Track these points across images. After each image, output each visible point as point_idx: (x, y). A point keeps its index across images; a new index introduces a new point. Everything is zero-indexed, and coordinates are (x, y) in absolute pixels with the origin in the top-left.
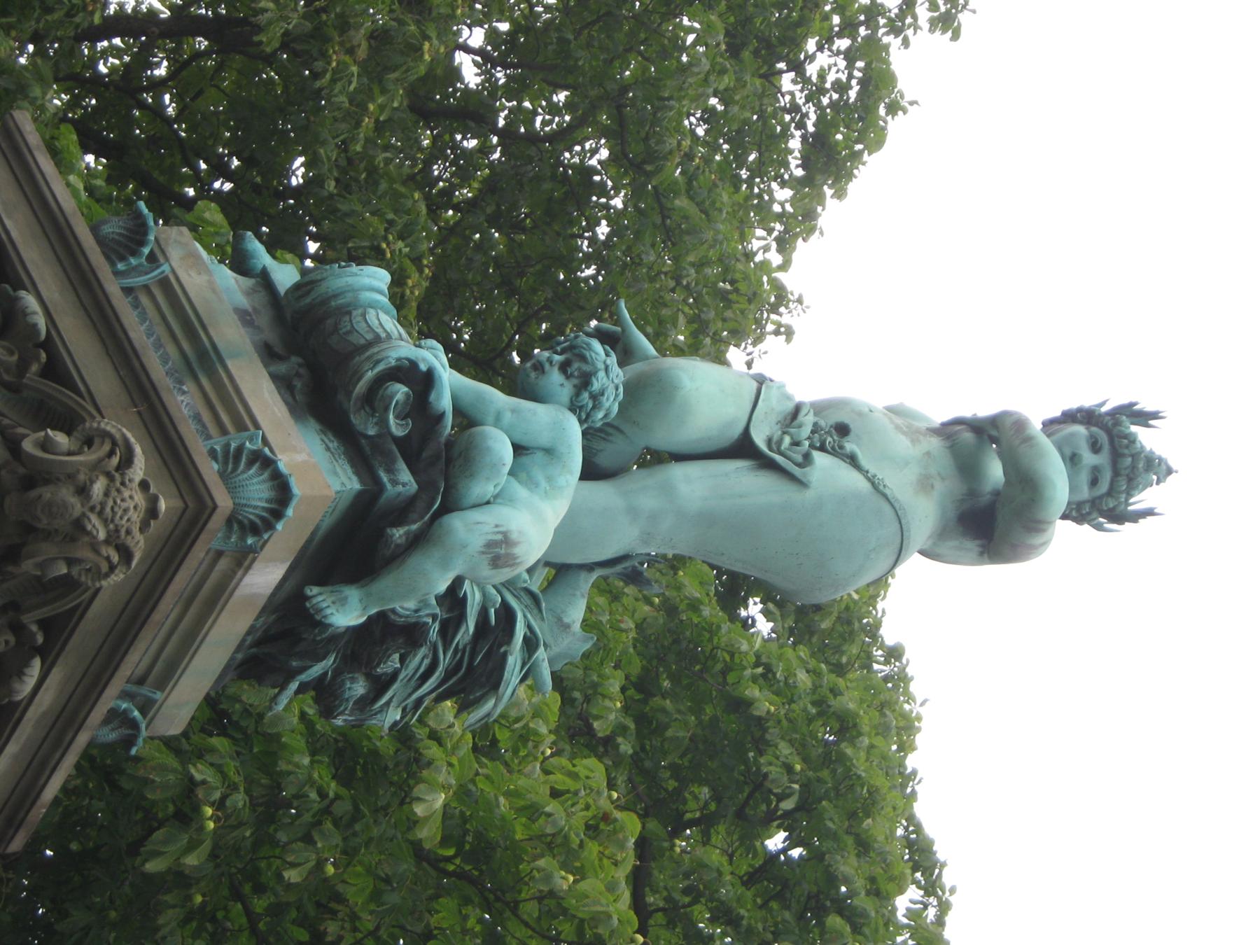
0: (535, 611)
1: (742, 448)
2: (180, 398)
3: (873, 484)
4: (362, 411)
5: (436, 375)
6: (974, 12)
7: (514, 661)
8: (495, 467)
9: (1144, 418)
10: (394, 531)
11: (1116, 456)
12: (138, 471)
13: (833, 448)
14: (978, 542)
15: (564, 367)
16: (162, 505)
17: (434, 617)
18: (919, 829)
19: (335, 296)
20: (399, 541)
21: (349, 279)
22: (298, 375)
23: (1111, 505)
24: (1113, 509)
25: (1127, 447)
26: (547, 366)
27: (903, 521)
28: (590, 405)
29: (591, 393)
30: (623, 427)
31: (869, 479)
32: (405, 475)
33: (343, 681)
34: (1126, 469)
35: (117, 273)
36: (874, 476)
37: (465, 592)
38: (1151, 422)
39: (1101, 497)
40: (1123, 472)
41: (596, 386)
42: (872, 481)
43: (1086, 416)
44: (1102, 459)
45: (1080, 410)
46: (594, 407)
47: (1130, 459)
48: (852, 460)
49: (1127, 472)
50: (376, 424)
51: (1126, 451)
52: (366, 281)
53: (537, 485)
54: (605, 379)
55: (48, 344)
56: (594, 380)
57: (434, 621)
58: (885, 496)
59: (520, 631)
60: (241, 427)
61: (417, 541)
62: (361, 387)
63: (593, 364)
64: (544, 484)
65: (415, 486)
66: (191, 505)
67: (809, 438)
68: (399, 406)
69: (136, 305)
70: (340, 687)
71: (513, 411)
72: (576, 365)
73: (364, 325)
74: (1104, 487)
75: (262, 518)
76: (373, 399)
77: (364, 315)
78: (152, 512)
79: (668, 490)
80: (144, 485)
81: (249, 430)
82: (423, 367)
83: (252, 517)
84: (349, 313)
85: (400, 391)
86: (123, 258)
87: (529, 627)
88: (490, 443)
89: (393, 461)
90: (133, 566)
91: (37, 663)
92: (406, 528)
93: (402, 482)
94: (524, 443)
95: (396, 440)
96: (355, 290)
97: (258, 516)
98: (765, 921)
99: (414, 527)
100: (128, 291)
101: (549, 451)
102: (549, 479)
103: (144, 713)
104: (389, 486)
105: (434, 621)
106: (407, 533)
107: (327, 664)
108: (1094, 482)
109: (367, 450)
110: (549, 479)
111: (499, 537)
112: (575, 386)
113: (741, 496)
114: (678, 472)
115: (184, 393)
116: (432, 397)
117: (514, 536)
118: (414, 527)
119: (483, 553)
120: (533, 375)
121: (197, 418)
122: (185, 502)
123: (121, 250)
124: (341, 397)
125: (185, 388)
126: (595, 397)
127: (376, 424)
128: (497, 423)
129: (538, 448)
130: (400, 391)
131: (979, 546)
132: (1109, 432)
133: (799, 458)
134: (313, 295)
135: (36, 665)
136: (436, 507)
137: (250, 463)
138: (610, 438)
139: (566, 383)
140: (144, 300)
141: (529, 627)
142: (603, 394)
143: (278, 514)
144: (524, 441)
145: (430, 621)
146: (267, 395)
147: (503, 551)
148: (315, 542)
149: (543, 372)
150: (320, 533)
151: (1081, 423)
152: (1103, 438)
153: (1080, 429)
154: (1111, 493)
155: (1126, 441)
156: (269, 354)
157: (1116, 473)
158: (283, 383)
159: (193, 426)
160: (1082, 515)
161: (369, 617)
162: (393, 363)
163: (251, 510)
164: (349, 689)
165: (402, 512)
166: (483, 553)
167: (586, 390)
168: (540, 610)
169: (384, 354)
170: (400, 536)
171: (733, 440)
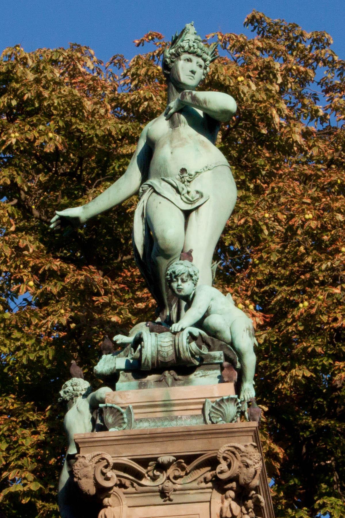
1: (187, 214)
11: (194, 53)
12: (242, 448)
15: (183, 281)
55: (178, 457)
80: (246, 446)
137: (220, 406)
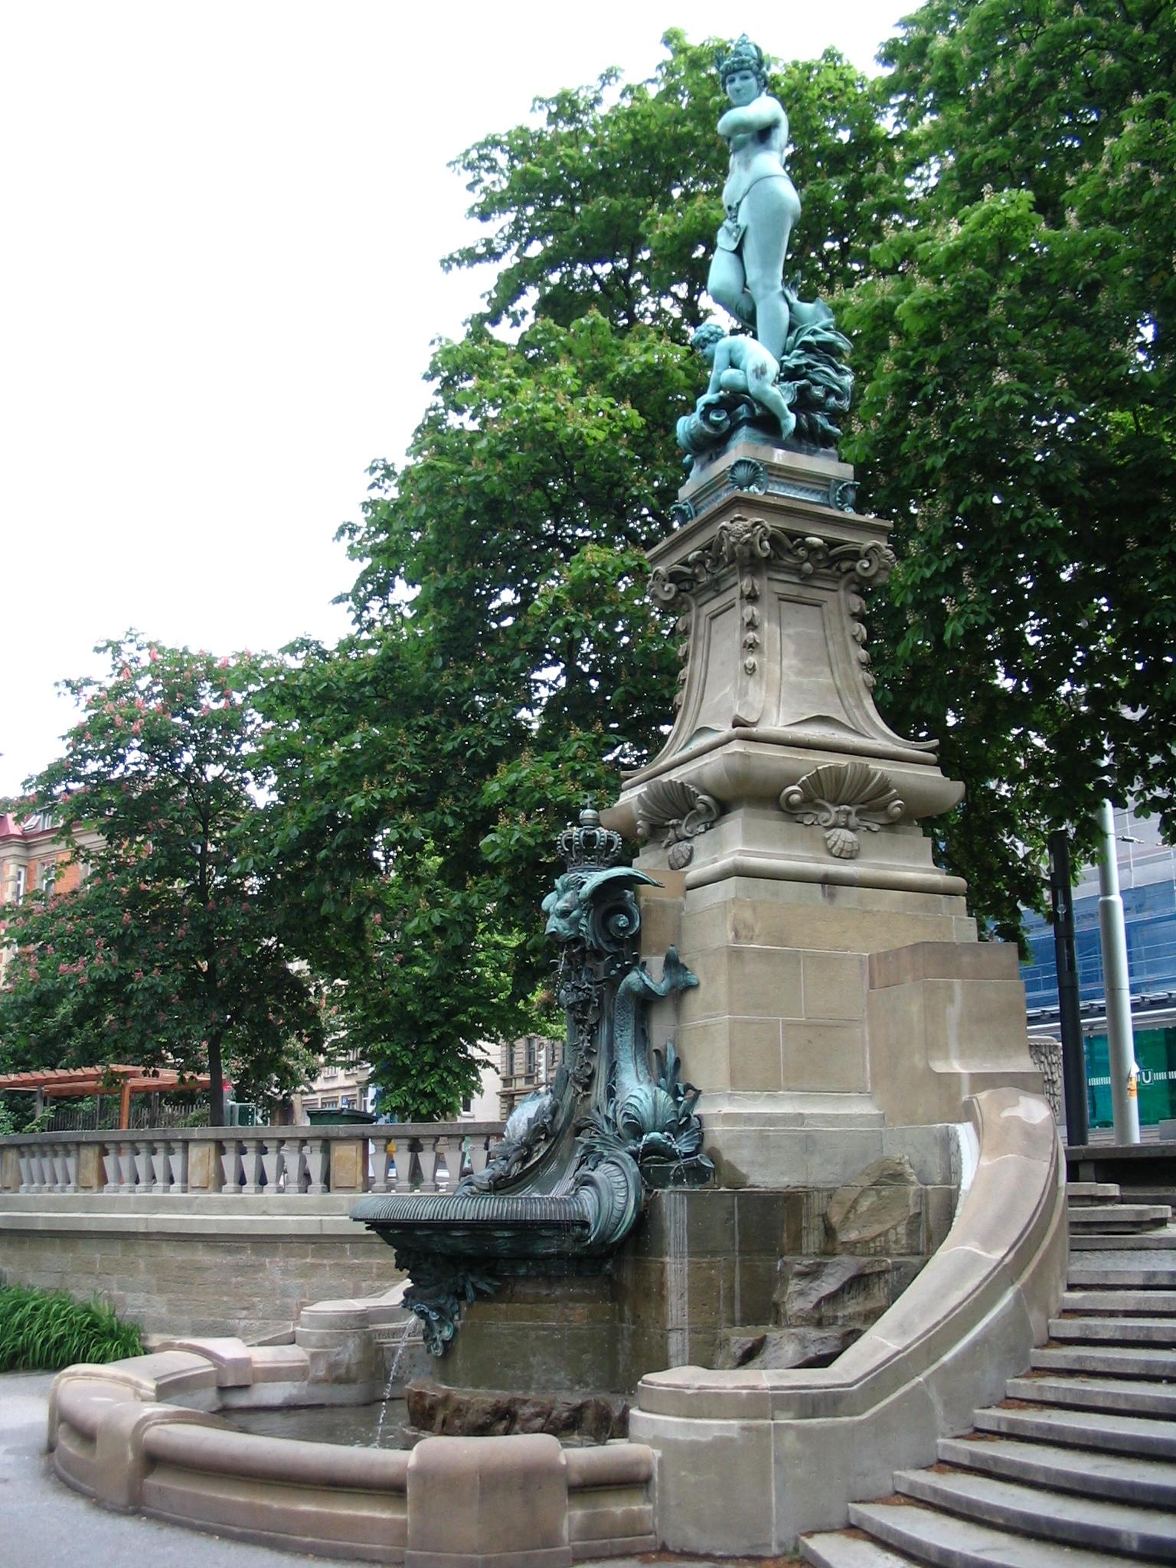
6: (97, 650)
7: (819, 338)
8: (732, 377)
11: (735, 71)
18: (250, 669)
42: (745, 195)
44: (737, 76)
48: (738, 204)
59: (810, 338)
61: (761, 404)
74: (749, 73)
76: (715, 425)
78: (739, 519)
79: (755, 283)
91: (809, 539)
93: (742, 409)
98: (339, 709)
101: (730, 351)
107: (820, 418)
108: (746, 78)
114: (749, 280)
126: (712, 334)
130: (713, 417)
135: (809, 539)
143: (749, 463)
144: (727, 361)
154: (750, 68)
157: (741, 69)
158: (718, 456)
165: (751, 409)
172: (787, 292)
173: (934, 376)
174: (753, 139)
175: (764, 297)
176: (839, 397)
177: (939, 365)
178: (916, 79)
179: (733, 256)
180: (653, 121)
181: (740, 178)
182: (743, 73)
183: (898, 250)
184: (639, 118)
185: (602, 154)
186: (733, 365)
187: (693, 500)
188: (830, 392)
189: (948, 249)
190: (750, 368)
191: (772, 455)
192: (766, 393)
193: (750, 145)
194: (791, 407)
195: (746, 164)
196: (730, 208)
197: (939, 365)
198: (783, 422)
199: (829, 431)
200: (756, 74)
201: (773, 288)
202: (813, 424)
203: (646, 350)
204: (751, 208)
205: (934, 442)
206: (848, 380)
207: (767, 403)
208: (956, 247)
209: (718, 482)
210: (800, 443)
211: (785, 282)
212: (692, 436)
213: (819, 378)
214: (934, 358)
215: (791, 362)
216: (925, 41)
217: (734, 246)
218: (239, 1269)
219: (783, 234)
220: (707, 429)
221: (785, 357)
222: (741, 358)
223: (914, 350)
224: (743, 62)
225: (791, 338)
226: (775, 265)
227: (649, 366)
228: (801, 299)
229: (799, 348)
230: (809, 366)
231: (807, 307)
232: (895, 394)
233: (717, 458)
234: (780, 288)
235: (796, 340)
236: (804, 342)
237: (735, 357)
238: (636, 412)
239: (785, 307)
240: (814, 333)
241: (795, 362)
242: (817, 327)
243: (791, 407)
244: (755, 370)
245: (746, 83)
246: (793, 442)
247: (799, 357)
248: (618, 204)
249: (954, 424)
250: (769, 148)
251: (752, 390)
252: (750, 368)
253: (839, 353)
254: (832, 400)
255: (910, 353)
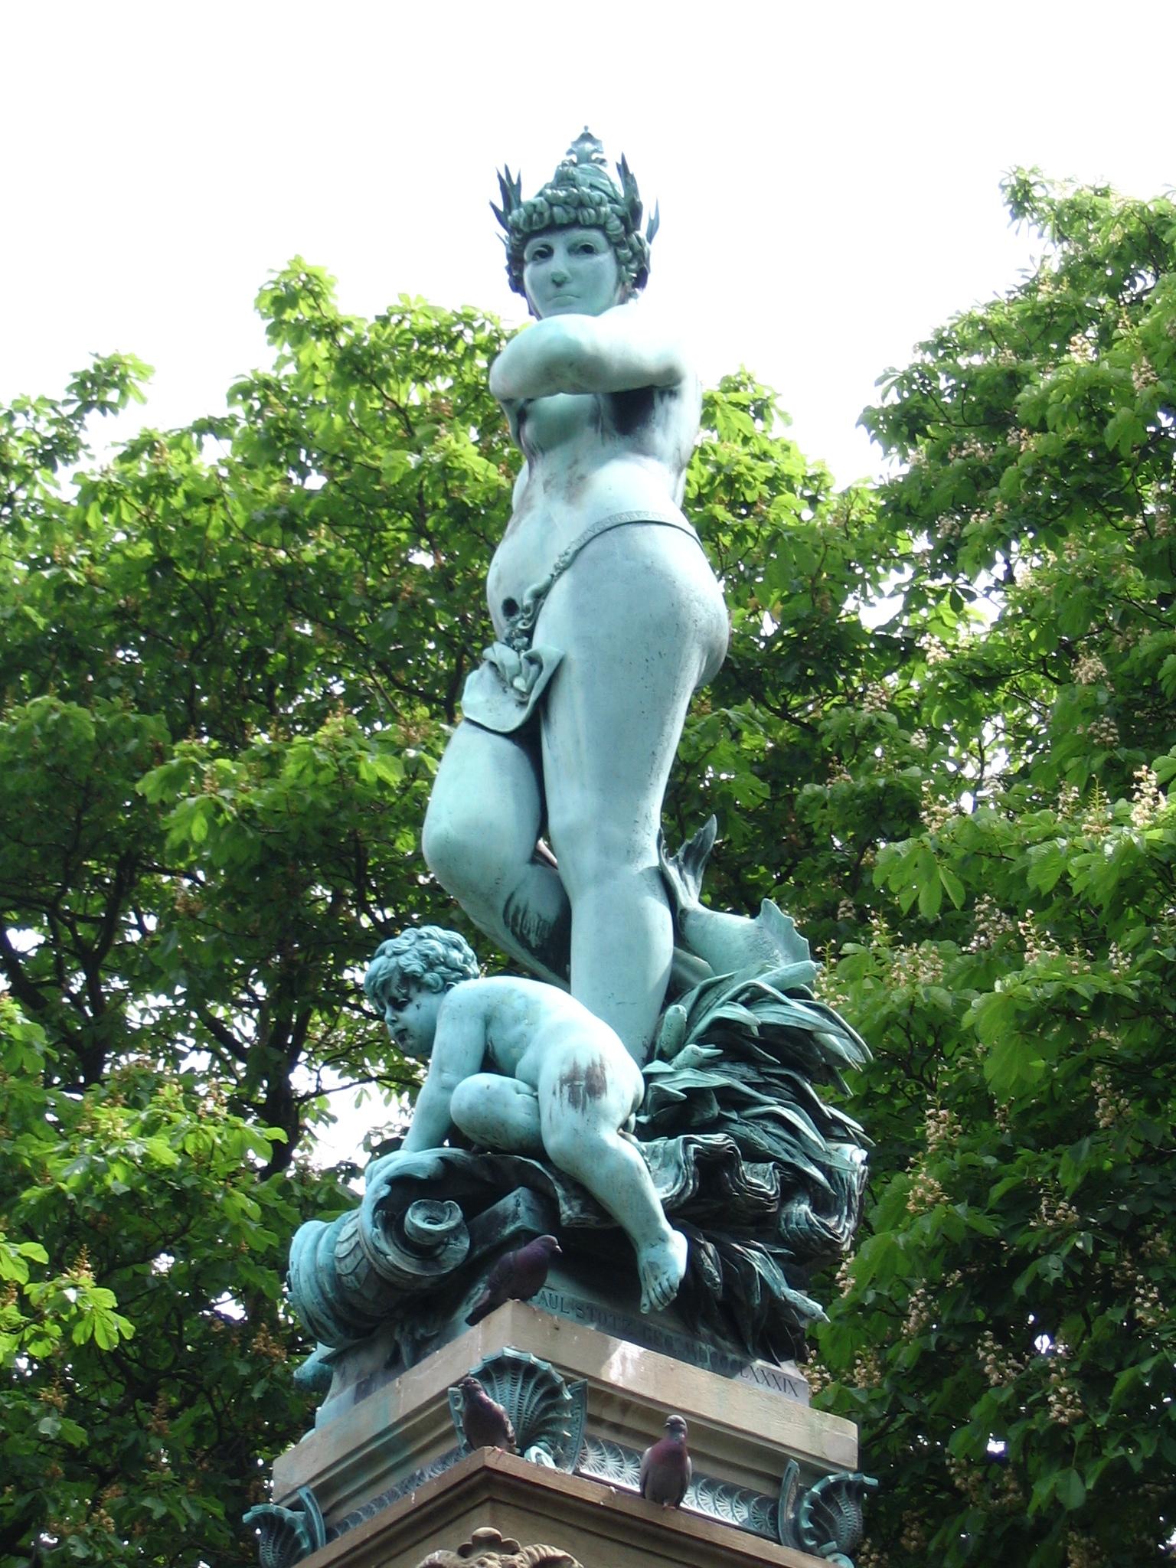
0: (722, 987)
2: (427, 1479)
3: (564, 569)
4: (443, 1257)
5: (397, 1173)
7: (769, 1015)
8: (491, 1097)
9: (510, 190)
10: (564, 1216)
11: (553, 227)
13: (529, 619)
14: (657, 400)
15: (399, 1006)
16: (483, 1530)
17: (687, 1142)
19: (323, 1293)
20: (577, 1209)
21: (302, 1279)
22: (412, 1332)
23: (618, 222)
24: (623, 220)
25: (541, 214)
26: (399, 1026)
27: (608, 525)
28: (442, 969)
29: (426, 971)
30: (506, 896)
31: (560, 574)
32: (508, 1202)
33: (789, 1232)
34: (567, 213)
35: (314, 1547)
36: (556, 568)
37: (682, 1091)
38: (515, 182)
39: (608, 238)
40: (573, 215)
41: (416, 966)
42: (561, 570)
43: (516, 263)
44: (559, 243)
45: (509, 270)
46: (444, 964)
47: (556, 209)
48: (540, 596)
49: (572, 210)
50: (456, 1239)
51: (547, 215)
52: (305, 1257)
53: (523, 1035)
54: (408, 955)
56: (408, 970)
57: (693, 1141)
58: (577, 553)
59: (737, 1012)
60: (445, 1413)
61: (579, 1188)
62: (407, 1265)
63: (392, 971)
64: (521, 1027)
65: (520, 1190)
66: (486, 1496)
67: (518, 651)
68: (434, 1215)
69: (344, 1526)
70: (797, 1235)
71: (441, 1071)
72: (395, 992)
73: (348, 1260)
74: (595, 237)
75: (537, 1387)
76: (423, 1248)
77: (341, 1260)
79: (573, 834)
81: (448, 1404)
82: (385, 1191)
83: (536, 1399)
84: (340, 1275)
85: (416, 1219)
86: (297, 1543)
87: (734, 999)
88: (464, 1105)
89: (496, 1214)
90: (560, 1553)
92: (561, 1202)
93: (516, 1203)
94: (480, 1052)
95: (467, 1218)
96: (317, 1270)
97: (533, 1393)
99: (560, 1192)
100: (330, 1535)
101: (488, 1021)
102: (517, 1020)
103: (820, 1474)
104: (518, 1224)
105: (693, 1141)
106: (568, 1202)
107: (760, 1262)
108: (588, 250)
109: (485, 1247)
110: (517, 1020)
111: (566, 1089)
112: (419, 991)
113: (578, 742)
114: (555, 822)
115: (422, 1474)
116: (421, 1175)
117: (566, 1070)
118: (560, 1192)
119: (584, 1109)
120: (410, 1042)
121: (444, 1461)
122: (486, 1500)
123: (291, 1542)
124: (425, 1285)
125: (418, 1473)
126: (431, 964)
127: (456, 1239)
128: (449, 1088)
129: (486, 1035)
130: (416, 1219)
131: (662, 400)
132: (526, 238)
133: (534, 668)
134: (324, 1319)
136: (538, 1165)
138: (522, 906)
139: (416, 1002)
140: (343, 1513)
141: (734, 999)
142: (427, 956)
143: (531, 1370)
144: (475, 1057)
145: (693, 1146)
146: (421, 1377)
147: (583, 1083)
148: (595, 1302)
149: (405, 1030)
150: (582, 1298)
151: (521, 271)
152: (535, 244)
153: (528, 272)
154: (602, 227)
155: (535, 216)
156: (395, 1364)
157: (575, 224)
158: (420, 1350)
159: (451, 1465)
160: (635, 254)
161: (675, 1228)
162: (379, 1230)
163: (525, 1403)
164: (797, 1224)
166: (584, 1109)
167: (422, 977)
168: (721, 981)
169: (369, 1242)
170: (571, 1208)
171: (522, 753)
172: (673, 872)
173: (1065, 1232)
174: (595, 419)
175: (602, 876)
176: (823, 1204)
177: (1083, 1199)
178: (982, 478)
179: (508, 747)
180: (219, 516)
181: (548, 520)
182: (579, 235)
183: (962, 867)
184: (178, 501)
185: (63, 589)
186: (490, 1063)
187: (323, 1491)
188: (795, 1183)
189: (1127, 851)
190: (551, 1072)
191: (604, 1356)
192: (601, 1151)
193: (588, 435)
194: (676, 1212)
195: (573, 487)
196: (510, 607)
197: (1083, 1199)
198: (646, 1255)
199: (789, 1305)
200: (616, 244)
201: (632, 853)
202: (738, 1273)
203: (150, 1129)
204: (580, 609)
205: (1059, 1428)
206: (852, 1157)
207: (599, 1190)
208: (1153, 847)
209: (408, 1438)
210: (692, 1330)
211: (670, 840)
212: (337, 1279)
213: (765, 1142)
214: (1071, 1180)
215: (679, 1079)
216: (1014, 380)
217: (515, 718)
218: (875, 1008)
219: (672, 695)
220: (393, 1255)
221: (657, 1066)
222: (522, 1043)
223: (1006, 1155)
224: (581, 203)
225: (680, 1009)
226: (642, 787)
227: (151, 1172)
228: (717, 900)
229: (701, 1041)
230: (728, 1097)
231: (734, 924)
232: (936, 1289)
233: (416, 1359)
234: (652, 857)
235: (691, 1021)
236: (720, 1023)
237: (502, 1039)
238: (107, 1298)
239: (661, 917)
240: (754, 997)
241: (690, 1079)
242: (762, 982)
243: (676, 1212)
244: (570, 1080)
245: (584, 263)
246: (670, 1328)
247: (704, 1065)
248: (86, 720)
249: (1124, 1378)
250: (643, 449)
251: (552, 1142)
252: (551, 1072)
253: (829, 1069)
254: (802, 1208)
255: (990, 1161)
